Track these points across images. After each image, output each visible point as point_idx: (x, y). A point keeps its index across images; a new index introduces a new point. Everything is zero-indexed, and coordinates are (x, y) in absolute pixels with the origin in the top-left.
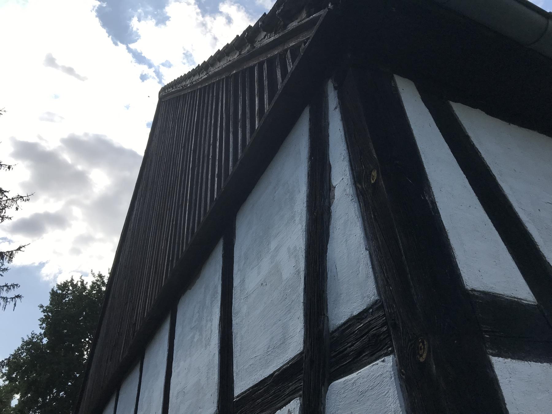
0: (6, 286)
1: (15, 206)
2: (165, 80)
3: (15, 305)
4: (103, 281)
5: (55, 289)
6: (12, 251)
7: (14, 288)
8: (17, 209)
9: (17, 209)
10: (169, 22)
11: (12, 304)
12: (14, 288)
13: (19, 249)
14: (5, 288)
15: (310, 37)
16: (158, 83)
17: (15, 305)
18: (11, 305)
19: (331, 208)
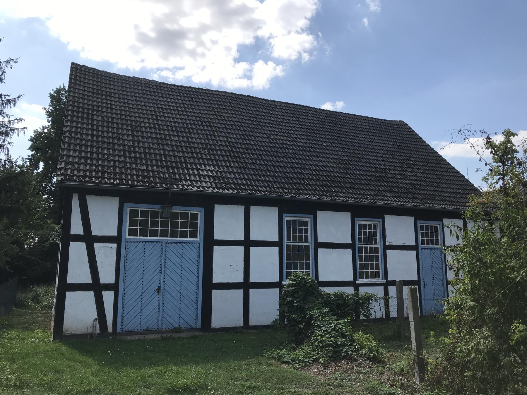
0: (16, 119)
1: (9, 66)
2: (60, 86)
3: (24, 133)
4: (45, 352)
5: (53, 93)
6: (15, 99)
7: (21, 121)
8: (11, 68)
9: (11, 68)
10: (265, 65)
11: (22, 132)
12: (21, 121)
13: (19, 97)
14: (16, 121)
15: (456, 234)
16: (49, 95)
17: (24, 133)
18: (22, 133)
19: (269, 323)
